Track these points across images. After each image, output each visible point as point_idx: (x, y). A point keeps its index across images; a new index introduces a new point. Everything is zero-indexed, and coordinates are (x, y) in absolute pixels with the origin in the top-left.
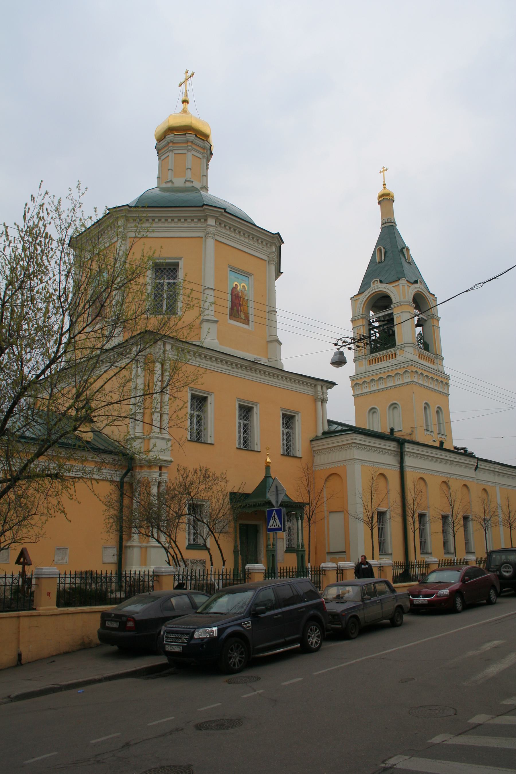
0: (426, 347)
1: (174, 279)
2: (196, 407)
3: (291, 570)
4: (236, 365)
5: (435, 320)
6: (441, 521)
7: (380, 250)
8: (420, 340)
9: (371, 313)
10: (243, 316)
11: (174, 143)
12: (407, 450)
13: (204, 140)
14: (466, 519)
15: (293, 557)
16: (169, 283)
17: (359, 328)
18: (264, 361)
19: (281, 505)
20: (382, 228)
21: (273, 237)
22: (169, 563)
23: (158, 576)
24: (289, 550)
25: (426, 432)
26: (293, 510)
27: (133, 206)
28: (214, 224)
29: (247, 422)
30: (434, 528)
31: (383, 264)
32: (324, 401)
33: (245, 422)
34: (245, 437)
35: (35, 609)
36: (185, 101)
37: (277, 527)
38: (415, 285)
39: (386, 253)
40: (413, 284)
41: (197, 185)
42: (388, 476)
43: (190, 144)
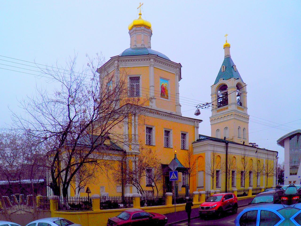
0: (241, 104)
1: (138, 83)
2: (148, 132)
3: (182, 195)
4: (163, 115)
5: (245, 94)
6: (240, 174)
7: (224, 67)
8: (238, 102)
9: (219, 92)
10: (166, 96)
11: (136, 30)
12: (229, 146)
13: (148, 29)
14: (250, 172)
15: (184, 188)
16: (136, 85)
17: (214, 98)
18: (174, 113)
19: (176, 170)
20: (225, 58)
21: (178, 65)
22: (138, 193)
23: (135, 198)
24: (183, 186)
25: (238, 138)
26: (185, 171)
27: (121, 56)
28: (153, 61)
29: (168, 137)
30: (238, 176)
31: (225, 72)
32: (197, 128)
33: (167, 137)
34: (167, 143)
35: (93, 210)
36: (140, 15)
37: (175, 178)
38: (238, 80)
39: (226, 68)
40: (236, 79)
41: (146, 46)
42: (221, 156)
43: (143, 31)
